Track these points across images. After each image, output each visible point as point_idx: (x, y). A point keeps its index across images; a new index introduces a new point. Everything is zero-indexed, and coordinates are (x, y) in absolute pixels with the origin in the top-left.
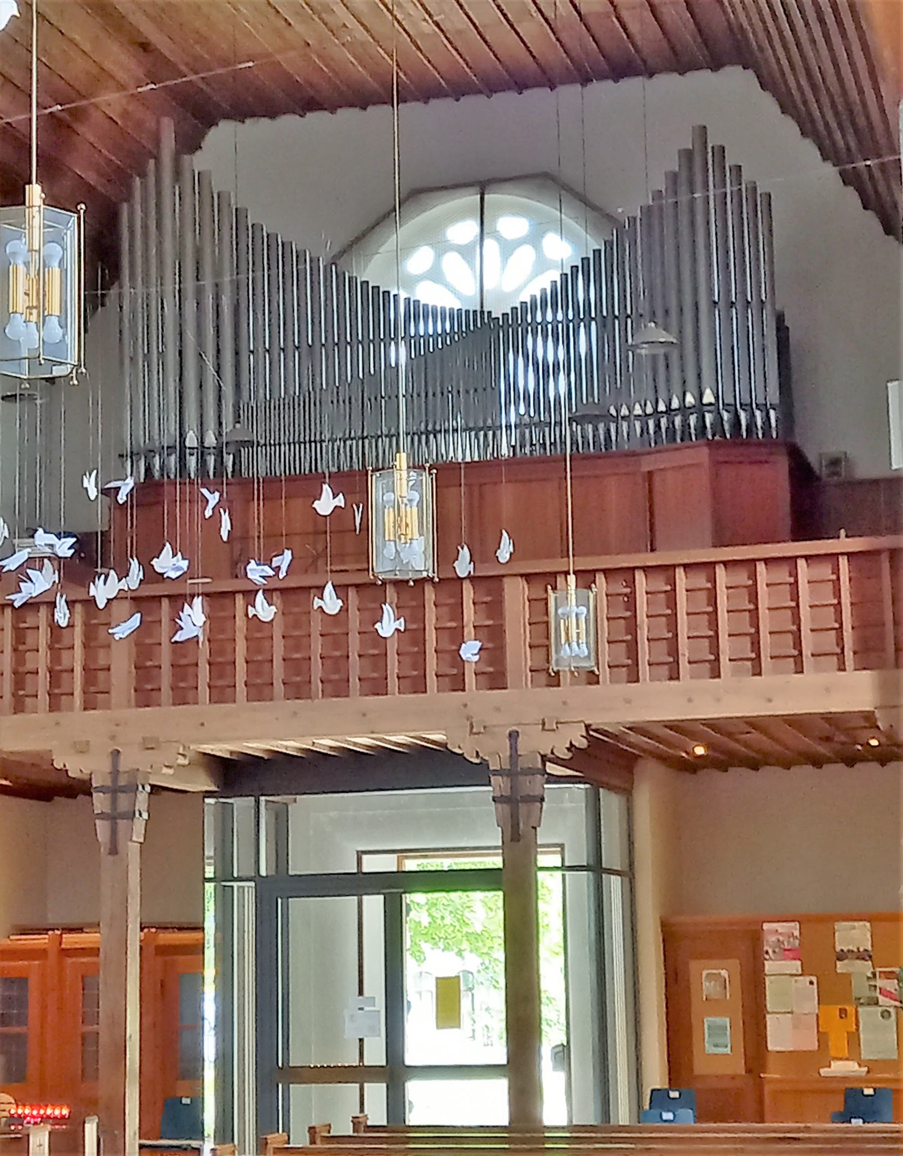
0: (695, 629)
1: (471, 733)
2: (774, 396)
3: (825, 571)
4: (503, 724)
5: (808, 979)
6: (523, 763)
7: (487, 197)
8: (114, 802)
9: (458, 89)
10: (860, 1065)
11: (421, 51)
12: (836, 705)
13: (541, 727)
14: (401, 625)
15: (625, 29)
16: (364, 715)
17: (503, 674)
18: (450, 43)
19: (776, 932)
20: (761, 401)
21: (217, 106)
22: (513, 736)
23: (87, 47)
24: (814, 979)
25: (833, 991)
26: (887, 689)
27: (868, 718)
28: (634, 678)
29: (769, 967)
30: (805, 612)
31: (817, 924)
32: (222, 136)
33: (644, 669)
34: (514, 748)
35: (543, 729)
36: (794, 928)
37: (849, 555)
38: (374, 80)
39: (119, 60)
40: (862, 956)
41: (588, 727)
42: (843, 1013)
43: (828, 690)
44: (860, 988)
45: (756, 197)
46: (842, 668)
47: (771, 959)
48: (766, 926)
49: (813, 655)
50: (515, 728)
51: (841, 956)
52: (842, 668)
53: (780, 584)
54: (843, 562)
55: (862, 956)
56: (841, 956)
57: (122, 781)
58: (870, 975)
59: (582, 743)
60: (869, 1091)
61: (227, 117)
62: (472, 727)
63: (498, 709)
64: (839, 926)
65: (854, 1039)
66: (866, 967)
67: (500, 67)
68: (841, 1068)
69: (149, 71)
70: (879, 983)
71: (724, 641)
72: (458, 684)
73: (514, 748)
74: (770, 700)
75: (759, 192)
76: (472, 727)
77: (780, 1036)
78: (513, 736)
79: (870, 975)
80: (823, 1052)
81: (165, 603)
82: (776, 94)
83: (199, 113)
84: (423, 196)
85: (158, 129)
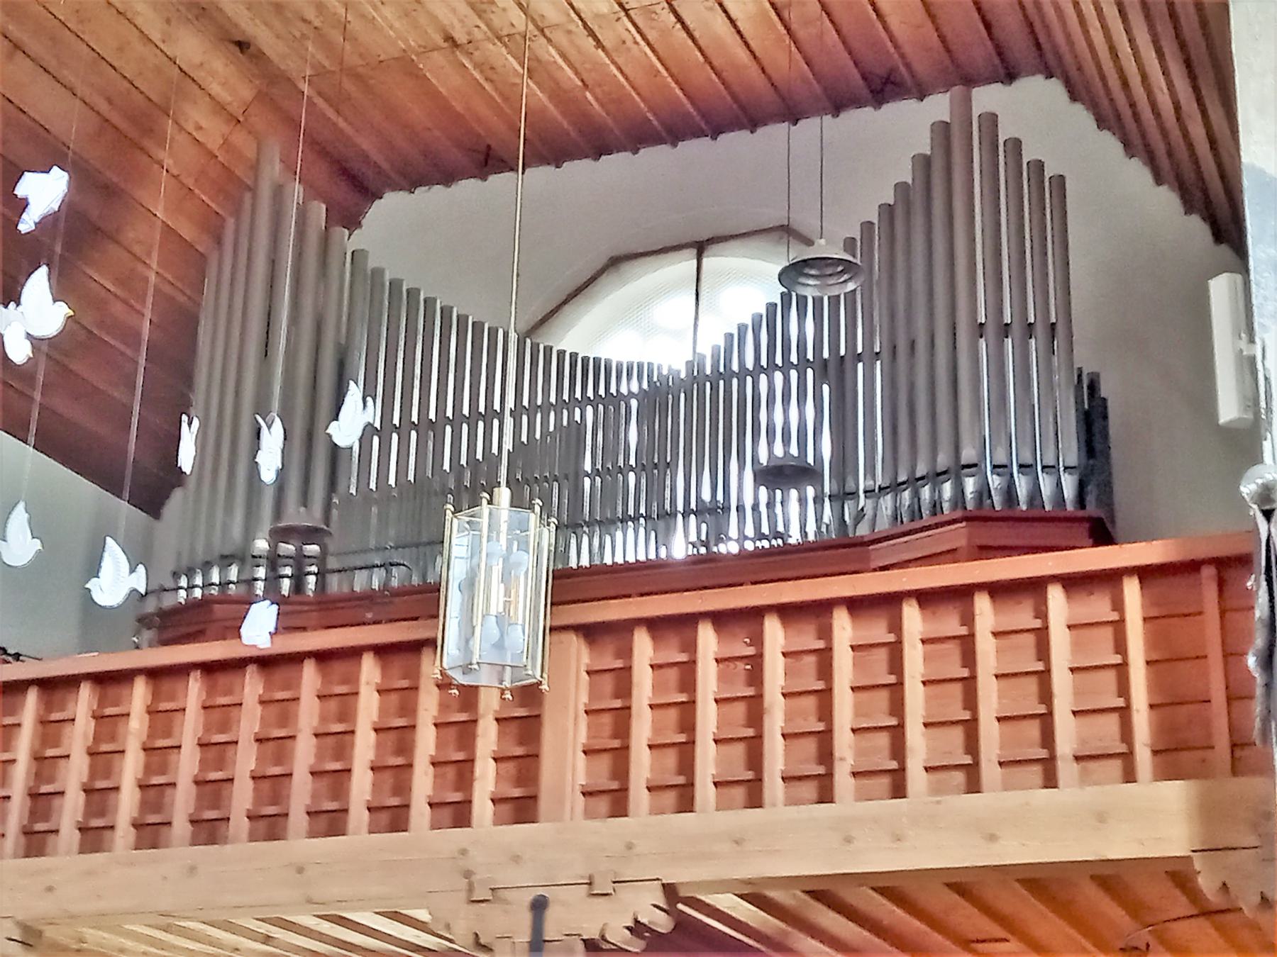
0: (866, 715)
2: (1071, 453)
3: (1098, 607)
4: (523, 881)
7: (705, 261)
9: (674, 131)
11: (604, 49)
12: (1119, 845)
14: (139, 581)
15: (886, 28)
16: (300, 870)
17: (534, 798)
18: (653, 51)
20: (1050, 461)
21: (379, 171)
22: (539, 906)
23: (156, 37)
26: (1209, 813)
27: (1178, 874)
28: (755, 800)
30: (1062, 681)
32: (390, 212)
33: (774, 787)
37: (1145, 573)
38: (564, 114)
39: (224, 78)
41: (670, 891)
43: (1101, 817)
45: (1043, 182)
46: (1129, 776)
49: (1078, 758)
50: (541, 891)
52: (1129, 776)
53: (1016, 632)
54: (1132, 590)
59: (663, 923)
61: (397, 187)
62: (471, 889)
63: (516, 859)
67: (725, 93)
69: (259, 92)
71: (915, 735)
72: (460, 814)
75: (1047, 175)
76: (471, 889)
78: (539, 906)
81: (32, 698)
82: (1094, 107)
83: (353, 186)
84: (626, 267)
85: (258, 160)
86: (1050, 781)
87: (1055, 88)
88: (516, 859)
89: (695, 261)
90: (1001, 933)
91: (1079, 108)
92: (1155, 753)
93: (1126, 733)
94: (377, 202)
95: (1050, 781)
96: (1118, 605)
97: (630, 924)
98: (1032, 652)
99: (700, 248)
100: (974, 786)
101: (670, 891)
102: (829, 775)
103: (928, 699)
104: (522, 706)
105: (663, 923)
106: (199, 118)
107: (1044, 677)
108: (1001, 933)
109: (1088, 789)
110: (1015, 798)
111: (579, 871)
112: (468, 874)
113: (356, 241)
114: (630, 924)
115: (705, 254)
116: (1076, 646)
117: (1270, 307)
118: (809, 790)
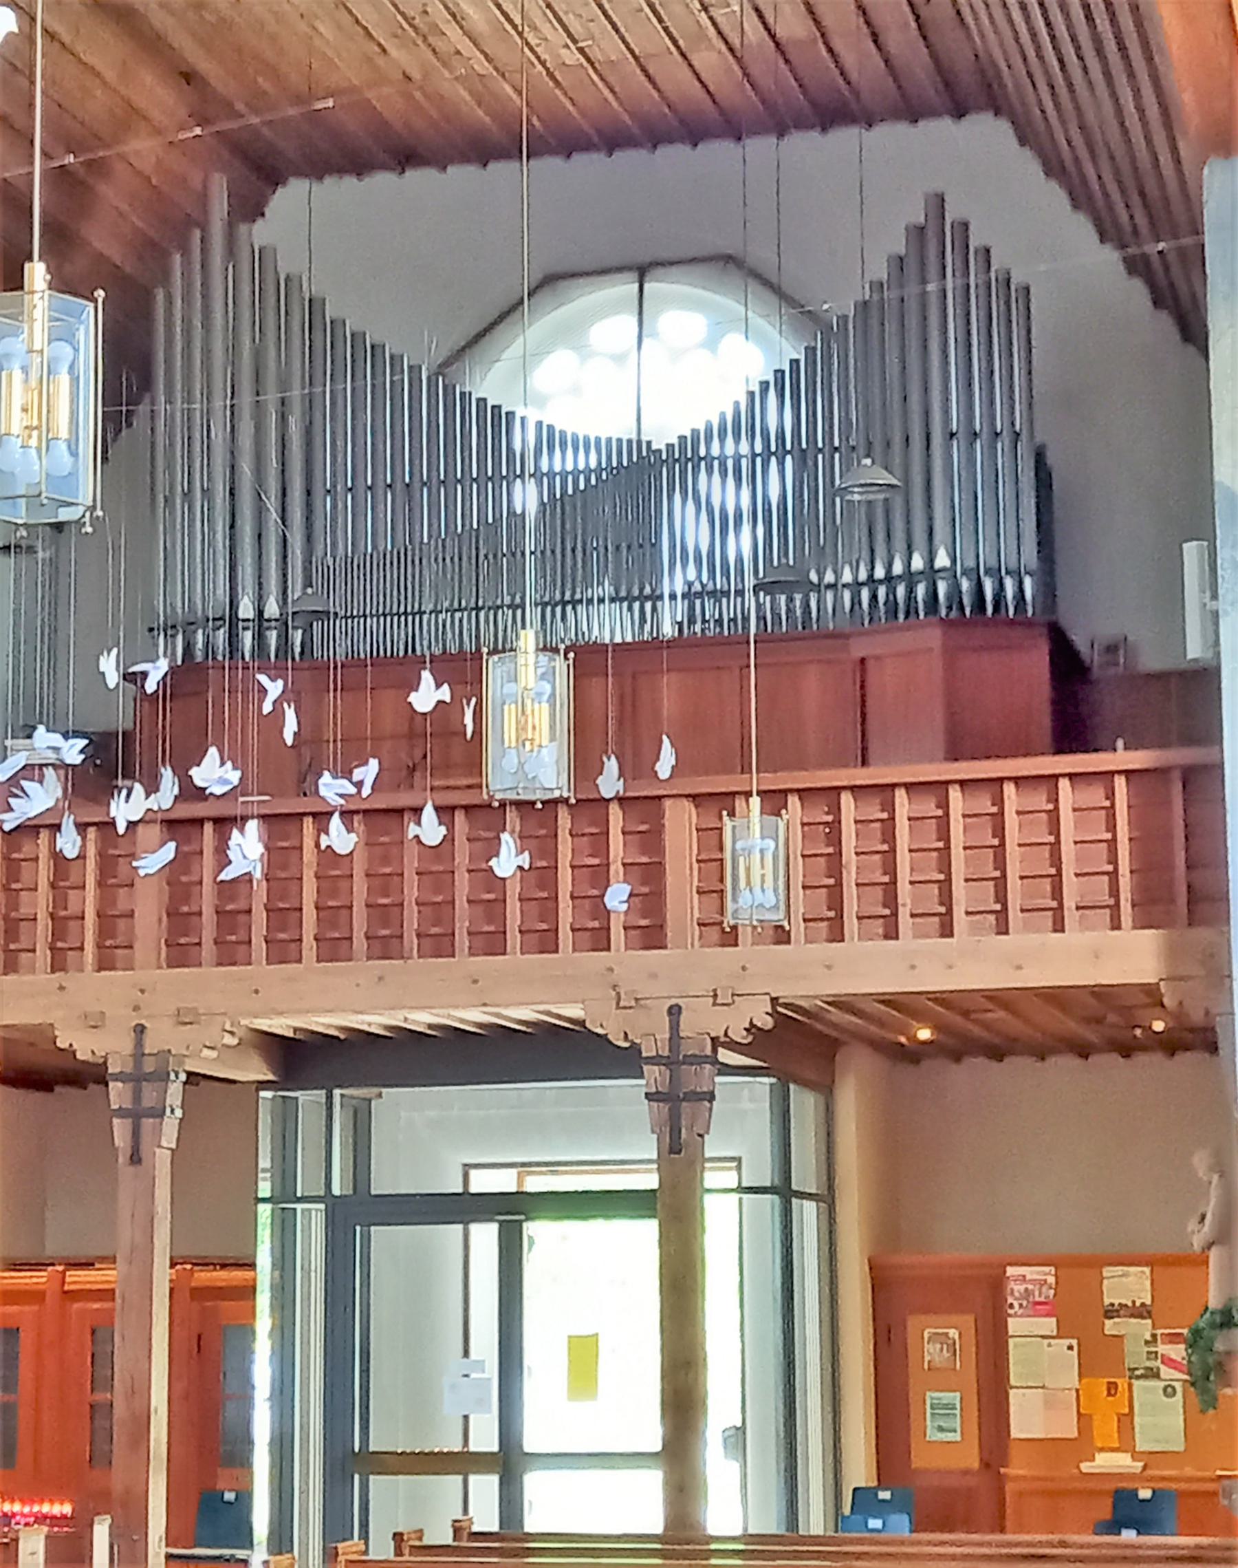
1: (618, 1007)
4: (661, 993)
5: (1067, 1342)
6: (689, 1049)
7: (646, 286)
8: (137, 1096)
10: (1134, 1459)
13: (711, 1000)
19: (1025, 1279)
24: (1074, 1342)
25: (1099, 1358)
26: (1172, 953)
28: (837, 935)
29: (1013, 1325)
31: (1080, 1268)
32: (291, 199)
33: (851, 924)
34: (675, 1027)
35: (714, 1004)
36: (1048, 1274)
39: (156, 95)
40: (1141, 1312)
41: (774, 1001)
42: (1112, 1389)
44: (1135, 1355)
46: (1116, 925)
47: (1016, 1315)
48: (1010, 1271)
50: (674, 1001)
51: (1111, 1312)
52: (1116, 925)
54: (1120, 783)
55: (1141, 1312)
56: (1111, 1312)
57: (149, 1066)
58: (1148, 1338)
60: (1145, 1494)
63: (654, 976)
64: (1107, 1271)
65: (1126, 1421)
66: (1144, 1327)
68: (1110, 1461)
70: (1162, 1349)
72: (601, 940)
73: (675, 1027)
74: (1019, 967)
77: (1028, 1418)
79: (1148, 1338)
80: (1083, 1444)
83: (260, 172)
86: (1059, 927)
87: (1003, 127)
88: (654, 976)
89: (636, 285)
90: (991, 1007)
91: (1027, 153)
92: (1133, 906)
93: (1115, 892)
94: (280, 190)
95: (1059, 927)
96: (1111, 795)
97: (747, 1026)
98: (1045, 828)
99: (642, 272)
100: (1003, 930)
101: (774, 1001)
102: (895, 914)
103: (967, 860)
104: (644, 854)
105: (769, 1023)
106: (142, 149)
107: (1056, 847)
108: (991, 1007)
109: (1087, 933)
110: (1034, 939)
111: (706, 987)
112: (614, 987)
113: (260, 233)
114: (747, 1026)
115: (647, 279)
116: (1077, 825)
117: (1230, 597)
118: (878, 927)
